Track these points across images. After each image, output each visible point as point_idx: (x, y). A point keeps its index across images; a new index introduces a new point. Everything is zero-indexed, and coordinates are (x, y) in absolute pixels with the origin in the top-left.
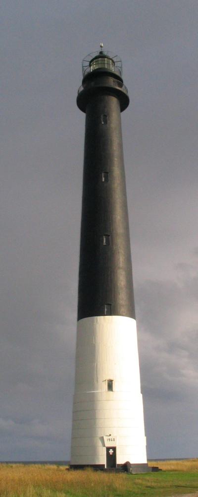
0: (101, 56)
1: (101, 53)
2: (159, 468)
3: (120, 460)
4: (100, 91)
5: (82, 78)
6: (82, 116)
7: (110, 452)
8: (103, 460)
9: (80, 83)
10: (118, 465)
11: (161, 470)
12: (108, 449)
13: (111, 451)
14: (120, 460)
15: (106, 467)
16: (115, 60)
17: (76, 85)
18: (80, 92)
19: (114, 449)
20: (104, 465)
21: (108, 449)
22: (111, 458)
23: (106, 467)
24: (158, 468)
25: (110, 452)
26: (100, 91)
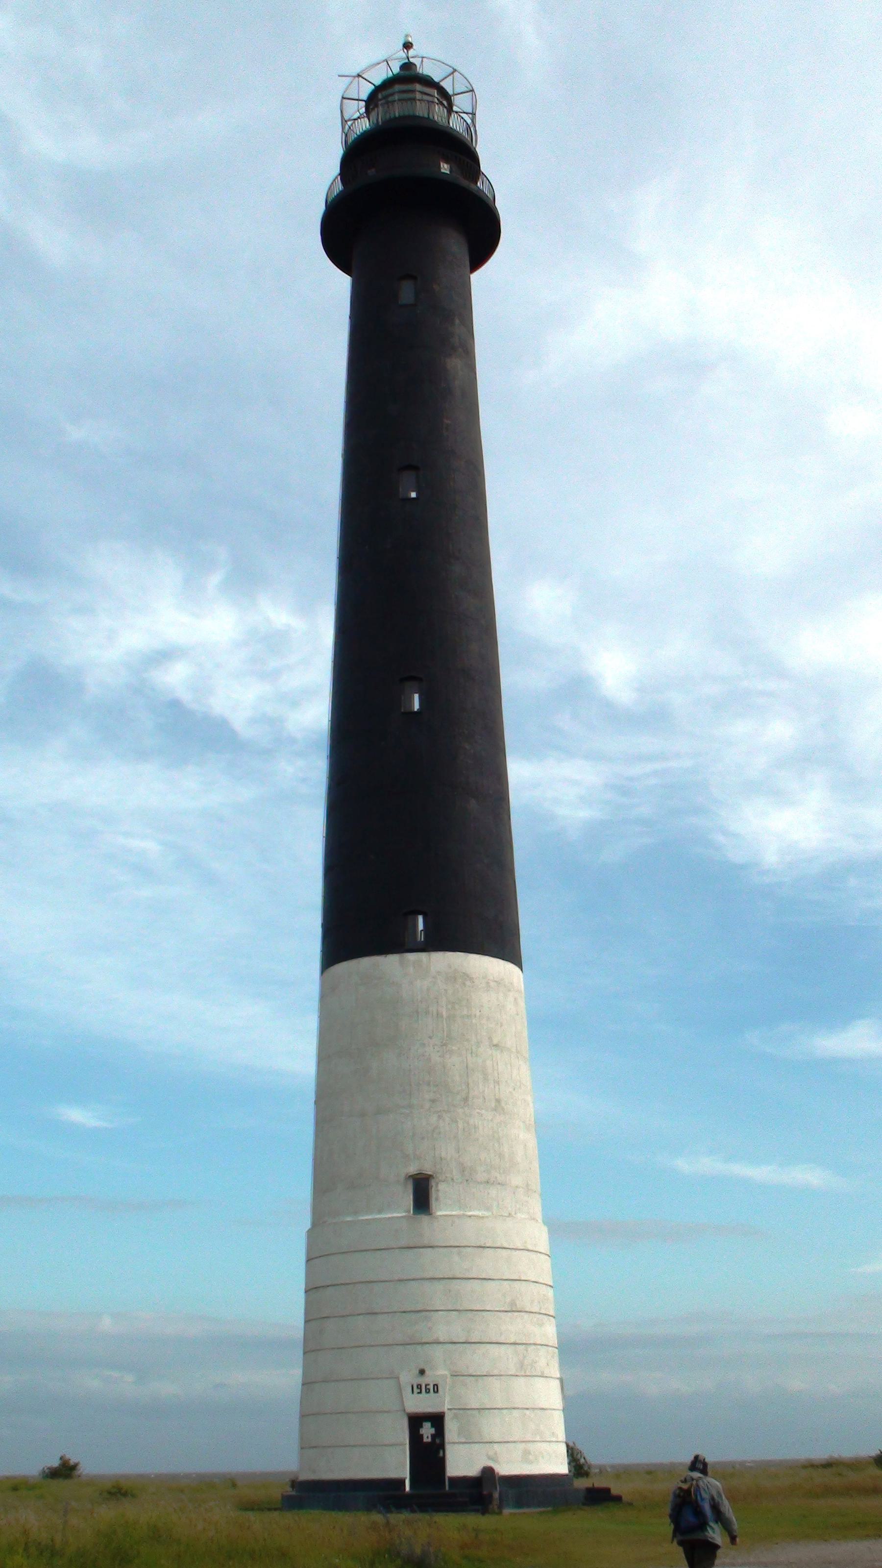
0: (408, 78)
1: (407, 66)
2: (614, 1492)
3: (461, 1462)
4: (409, 202)
5: (337, 152)
6: (341, 284)
7: (433, 1431)
8: (397, 1465)
9: (335, 169)
10: (570, 1471)
11: (618, 1499)
12: (415, 1421)
13: (427, 1431)
14: (461, 1462)
15: (408, 1488)
16: (447, 85)
17: (320, 172)
18: (329, 200)
19: (437, 1420)
20: (402, 1482)
21: (415, 1421)
22: (428, 1453)
23: (408, 1488)
24: (608, 1490)
25: (433, 1431)
26: (409, 202)
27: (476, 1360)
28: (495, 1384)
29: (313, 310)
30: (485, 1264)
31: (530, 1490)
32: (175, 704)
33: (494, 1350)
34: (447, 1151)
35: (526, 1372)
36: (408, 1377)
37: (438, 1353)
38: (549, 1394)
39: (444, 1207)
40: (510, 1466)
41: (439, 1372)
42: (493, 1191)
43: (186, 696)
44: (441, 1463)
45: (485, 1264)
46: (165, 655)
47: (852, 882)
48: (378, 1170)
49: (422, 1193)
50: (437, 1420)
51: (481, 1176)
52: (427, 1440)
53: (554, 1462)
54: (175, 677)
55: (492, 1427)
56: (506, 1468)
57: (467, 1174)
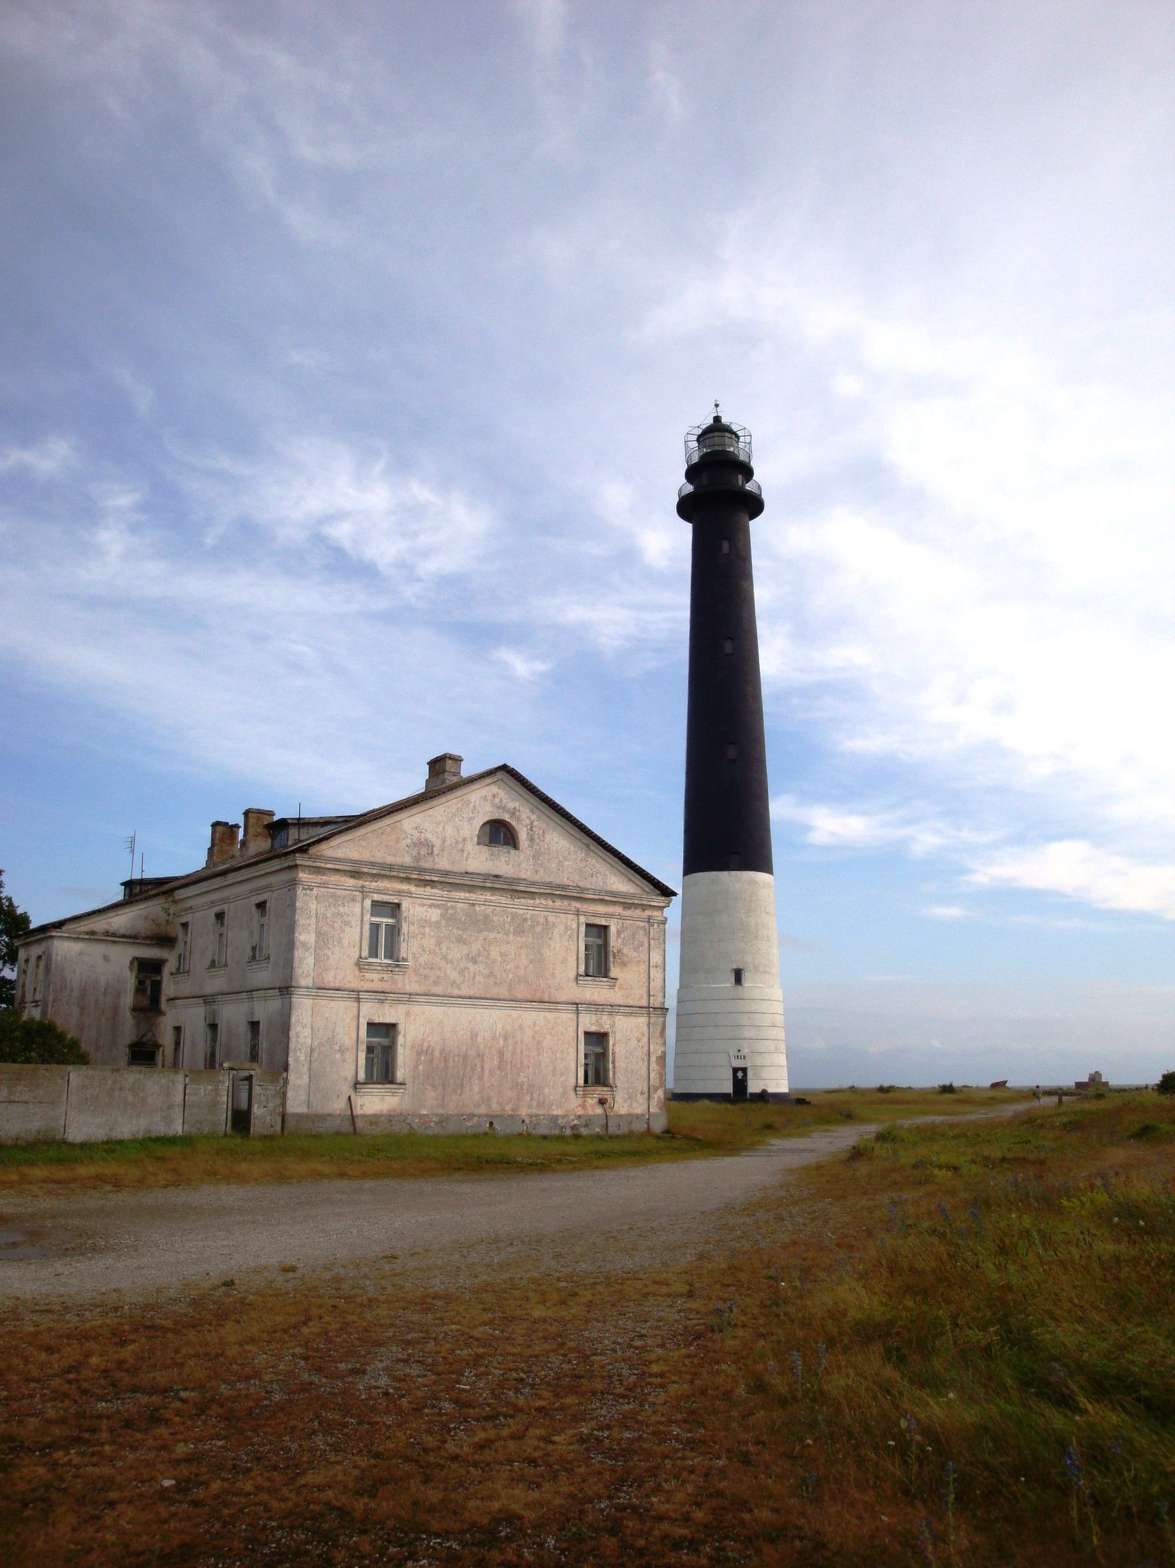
1: (717, 419)
3: (753, 1087)
4: (719, 494)
8: (728, 1087)
11: (809, 1103)
12: (735, 1070)
14: (753, 1087)
16: (739, 433)
19: (744, 1070)
21: (735, 1070)
26: (719, 494)
27: (761, 1046)
28: (767, 1056)
29: (671, 543)
30: (764, 1007)
31: (778, 1097)
32: (339, 551)
33: (766, 1043)
34: (749, 959)
35: (777, 1051)
36: (733, 1053)
37: (745, 1043)
38: (782, 1059)
39: (747, 982)
40: (772, 1089)
41: (745, 1051)
42: (767, 976)
43: (347, 544)
44: (745, 1087)
45: (764, 1007)
46: (339, 516)
47: (795, 701)
48: (720, 967)
49: (738, 976)
50: (744, 1070)
51: (762, 970)
52: (740, 1078)
53: (783, 1088)
54: (341, 532)
55: (765, 1073)
56: (770, 1091)
57: (756, 969)
